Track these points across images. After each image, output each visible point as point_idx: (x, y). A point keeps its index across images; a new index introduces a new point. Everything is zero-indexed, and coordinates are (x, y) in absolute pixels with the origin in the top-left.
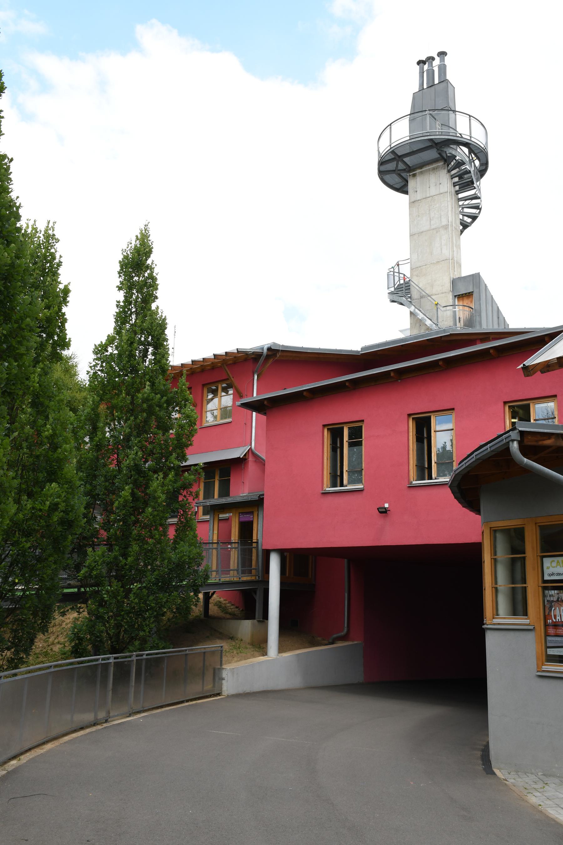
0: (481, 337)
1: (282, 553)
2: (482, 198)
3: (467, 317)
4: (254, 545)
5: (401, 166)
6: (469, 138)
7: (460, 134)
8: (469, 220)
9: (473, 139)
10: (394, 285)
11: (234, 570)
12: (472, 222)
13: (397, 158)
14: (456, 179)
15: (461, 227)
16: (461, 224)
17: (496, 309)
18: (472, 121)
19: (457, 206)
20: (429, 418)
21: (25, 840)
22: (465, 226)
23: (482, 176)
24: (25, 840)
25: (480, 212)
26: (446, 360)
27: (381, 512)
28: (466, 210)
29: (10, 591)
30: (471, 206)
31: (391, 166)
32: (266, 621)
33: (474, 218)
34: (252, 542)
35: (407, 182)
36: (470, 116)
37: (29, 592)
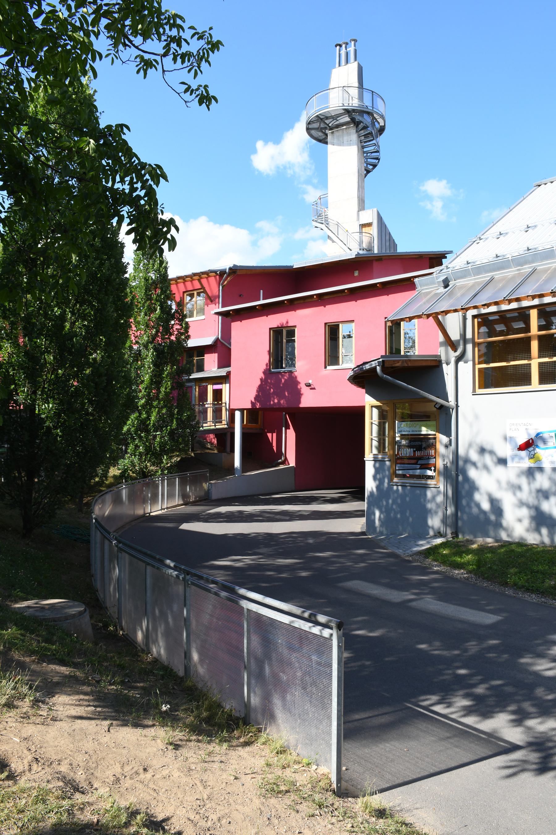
0: (376, 258)
1: (242, 410)
2: (381, 152)
3: (284, 699)
4: (224, 405)
5: (322, 125)
6: (371, 108)
7: (367, 106)
8: (371, 167)
9: (374, 109)
10: (317, 213)
11: (210, 422)
12: (373, 169)
13: (320, 120)
14: (363, 138)
15: (365, 172)
16: (365, 170)
17: (388, 237)
18: (374, 96)
19: (362, 158)
20: (338, 325)
21: (223, 762)
22: (368, 172)
23: (380, 134)
24: (223, 762)
25: (378, 162)
26: (350, 290)
27: (307, 386)
28: (369, 160)
29: (14, 353)
30: (372, 157)
31: (316, 125)
32: (232, 453)
33: (375, 166)
34: (222, 403)
35: (327, 136)
36: (373, 92)
37: (95, 480)
